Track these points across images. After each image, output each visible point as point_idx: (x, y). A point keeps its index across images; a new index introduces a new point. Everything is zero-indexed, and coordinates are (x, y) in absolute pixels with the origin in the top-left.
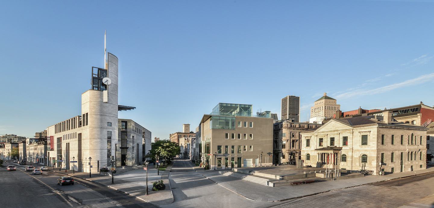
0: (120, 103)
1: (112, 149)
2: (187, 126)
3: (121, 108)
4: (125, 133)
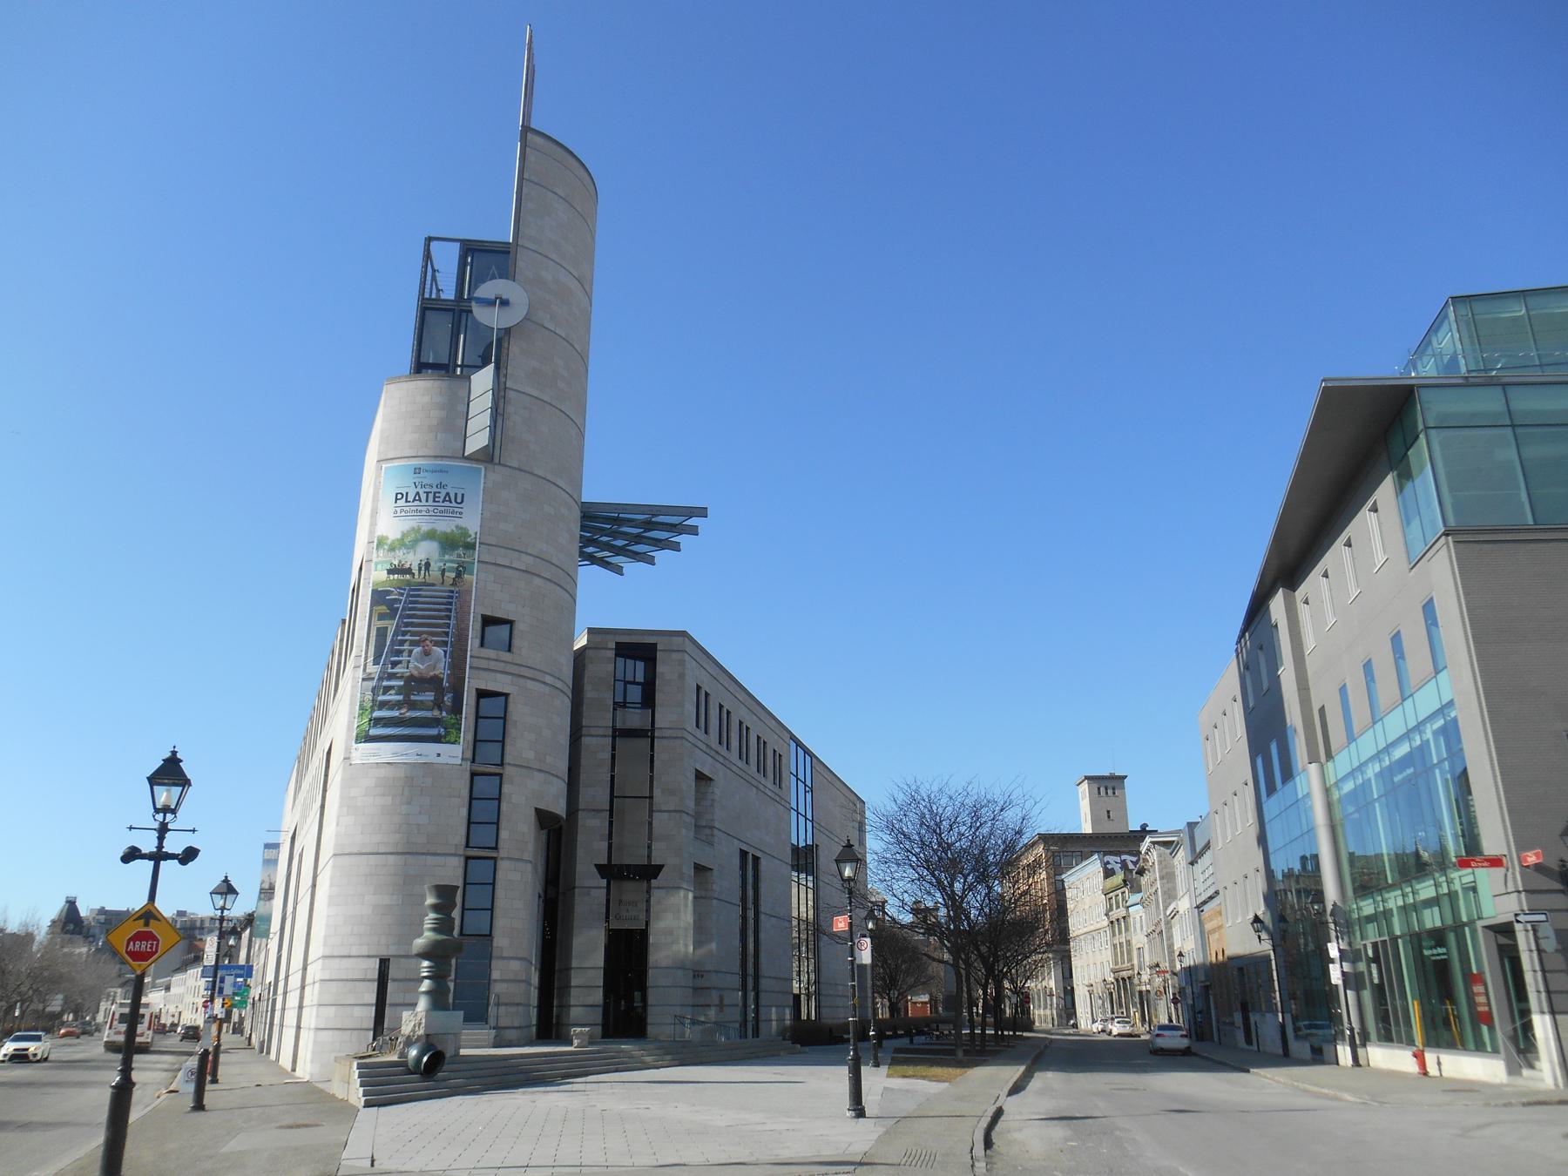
0: (608, 481)
1: (503, 853)
2: (1108, 785)
3: (618, 534)
4: (644, 743)
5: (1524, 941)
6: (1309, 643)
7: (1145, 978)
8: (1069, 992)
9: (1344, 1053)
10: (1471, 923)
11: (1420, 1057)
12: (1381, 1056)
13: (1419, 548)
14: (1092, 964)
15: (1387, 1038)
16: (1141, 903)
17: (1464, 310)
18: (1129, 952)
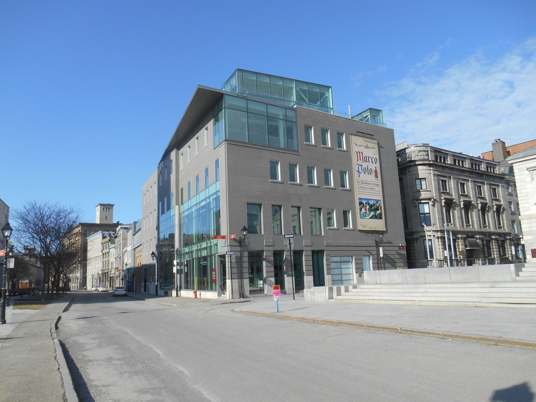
2: (107, 207)
5: (227, 259)
6: (181, 167)
7: (113, 272)
8: (84, 278)
9: (174, 293)
10: (215, 254)
11: (195, 293)
12: (184, 293)
13: (217, 144)
14: (94, 268)
15: (187, 288)
16: (114, 247)
17: (240, 74)
18: (108, 264)
